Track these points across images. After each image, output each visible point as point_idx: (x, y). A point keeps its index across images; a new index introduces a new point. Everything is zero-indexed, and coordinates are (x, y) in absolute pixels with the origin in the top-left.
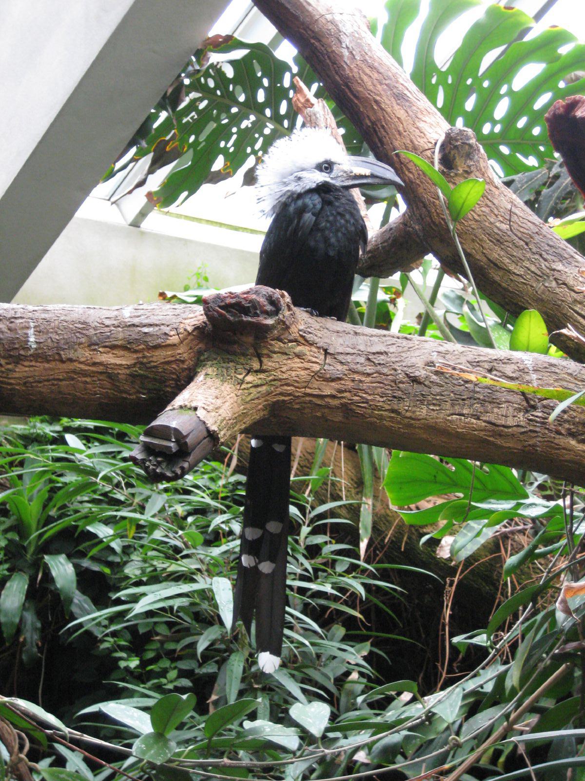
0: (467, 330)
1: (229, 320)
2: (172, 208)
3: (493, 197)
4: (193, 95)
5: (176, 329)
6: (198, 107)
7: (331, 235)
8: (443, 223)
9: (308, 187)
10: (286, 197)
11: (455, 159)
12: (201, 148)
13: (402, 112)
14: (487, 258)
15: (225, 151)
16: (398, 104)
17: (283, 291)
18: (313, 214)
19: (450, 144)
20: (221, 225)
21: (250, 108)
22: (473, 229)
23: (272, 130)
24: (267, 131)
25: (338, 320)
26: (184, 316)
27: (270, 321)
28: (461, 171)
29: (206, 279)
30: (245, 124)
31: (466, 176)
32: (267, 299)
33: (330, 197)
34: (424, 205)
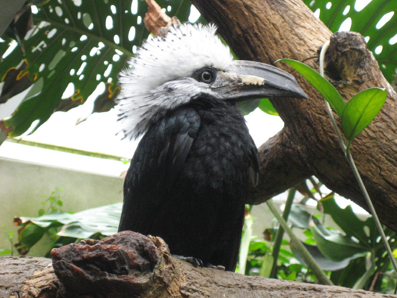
0: (314, 243)
1: (89, 282)
2: (24, 136)
3: (389, 110)
4: (43, 24)
5: (18, 292)
6: (46, 36)
7: (214, 162)
8: (332, 142)
9: (179, 102)
10: (153, 113)
11: (343, 68)
12: (52, 76)
13: (277, 17)
14: (387, 181)
15: (75, 79)
16: (272, 9)
17: (158, 238)
18: (190, 135)
19: (337, 50)
20: (73, 151)
21: (99, 35)
22: (368, 147)
23: (121, 57)
24: (116, 58)
25: (227, 269)
26: (28, 274)
27: (143, 280)
28: (350, 82)
29: (60, 203)
30: (94, 51)
31: (357, 86)
32: (137, 249)
33: (210, 114)
34: (309, 122)
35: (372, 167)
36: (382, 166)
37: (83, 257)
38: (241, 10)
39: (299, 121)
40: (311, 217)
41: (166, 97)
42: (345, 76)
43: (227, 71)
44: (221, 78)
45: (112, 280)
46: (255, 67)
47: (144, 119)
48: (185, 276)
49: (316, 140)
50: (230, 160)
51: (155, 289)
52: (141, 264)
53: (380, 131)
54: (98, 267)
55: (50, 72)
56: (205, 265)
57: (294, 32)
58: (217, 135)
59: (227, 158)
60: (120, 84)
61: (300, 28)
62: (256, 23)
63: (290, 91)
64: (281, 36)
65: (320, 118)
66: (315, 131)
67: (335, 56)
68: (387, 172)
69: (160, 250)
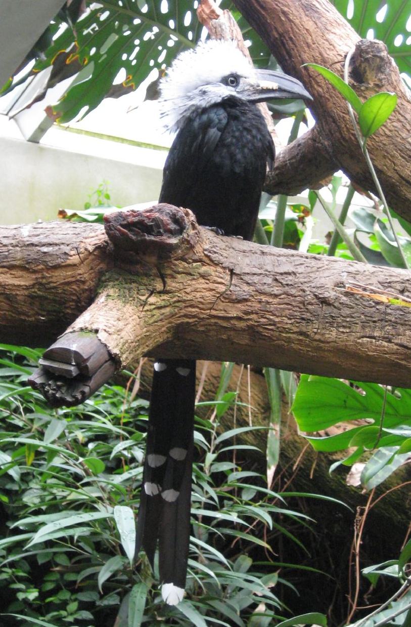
0: (378, 249)
2: (73, 123)
5: (77, 248)
6: (99, 18)
7: (237, 151)
9: (213, 102)
10: (190, 111)
13: (311, 23)
14: (399, 175)
15: (127, 64)
16: (307, 16)
18: (219, 129)
19: (361, 56)
20: (123, 140)
21: (154, 20)
22: (384, 144)
23: (176, 42)
24: (171, 43)
26: (85, 235)
27: (174, 241)
28: (371, 85)
29: (108, 197)
30: (148, 36)
31: (377, 89)
32: (171, 218)
33: (236, 112)
35: (387, 162)
36: (395, 162)
37: (128, 222)
38: (278, 15)
39: (326, 119)
40: (376, 221)
41: (201, 98)
42: (367, 79)
43: (248, 78)
44: (244, 83)
45: (150, 240)
46: (270, 75)
47: (184, 116)
48: (208, 240)
49: (340, 136)
50: (251, 150)
51: (184, 248)
52: (173, 229)
53: (395, 130)
54: (139, 229)
55: (102, 55)
56: (227, 234)
57: (325, 38)
58: (241, 129)
59: (248, 149)
60: (160, 89)
61: (331, 34)
62: (292, 28)
63: (298, 94)
64: (313, 41)
65: (344, 117)
66: (339, 128)
67: (359, 61)
68: (400, 167)
69: (189, 219)
